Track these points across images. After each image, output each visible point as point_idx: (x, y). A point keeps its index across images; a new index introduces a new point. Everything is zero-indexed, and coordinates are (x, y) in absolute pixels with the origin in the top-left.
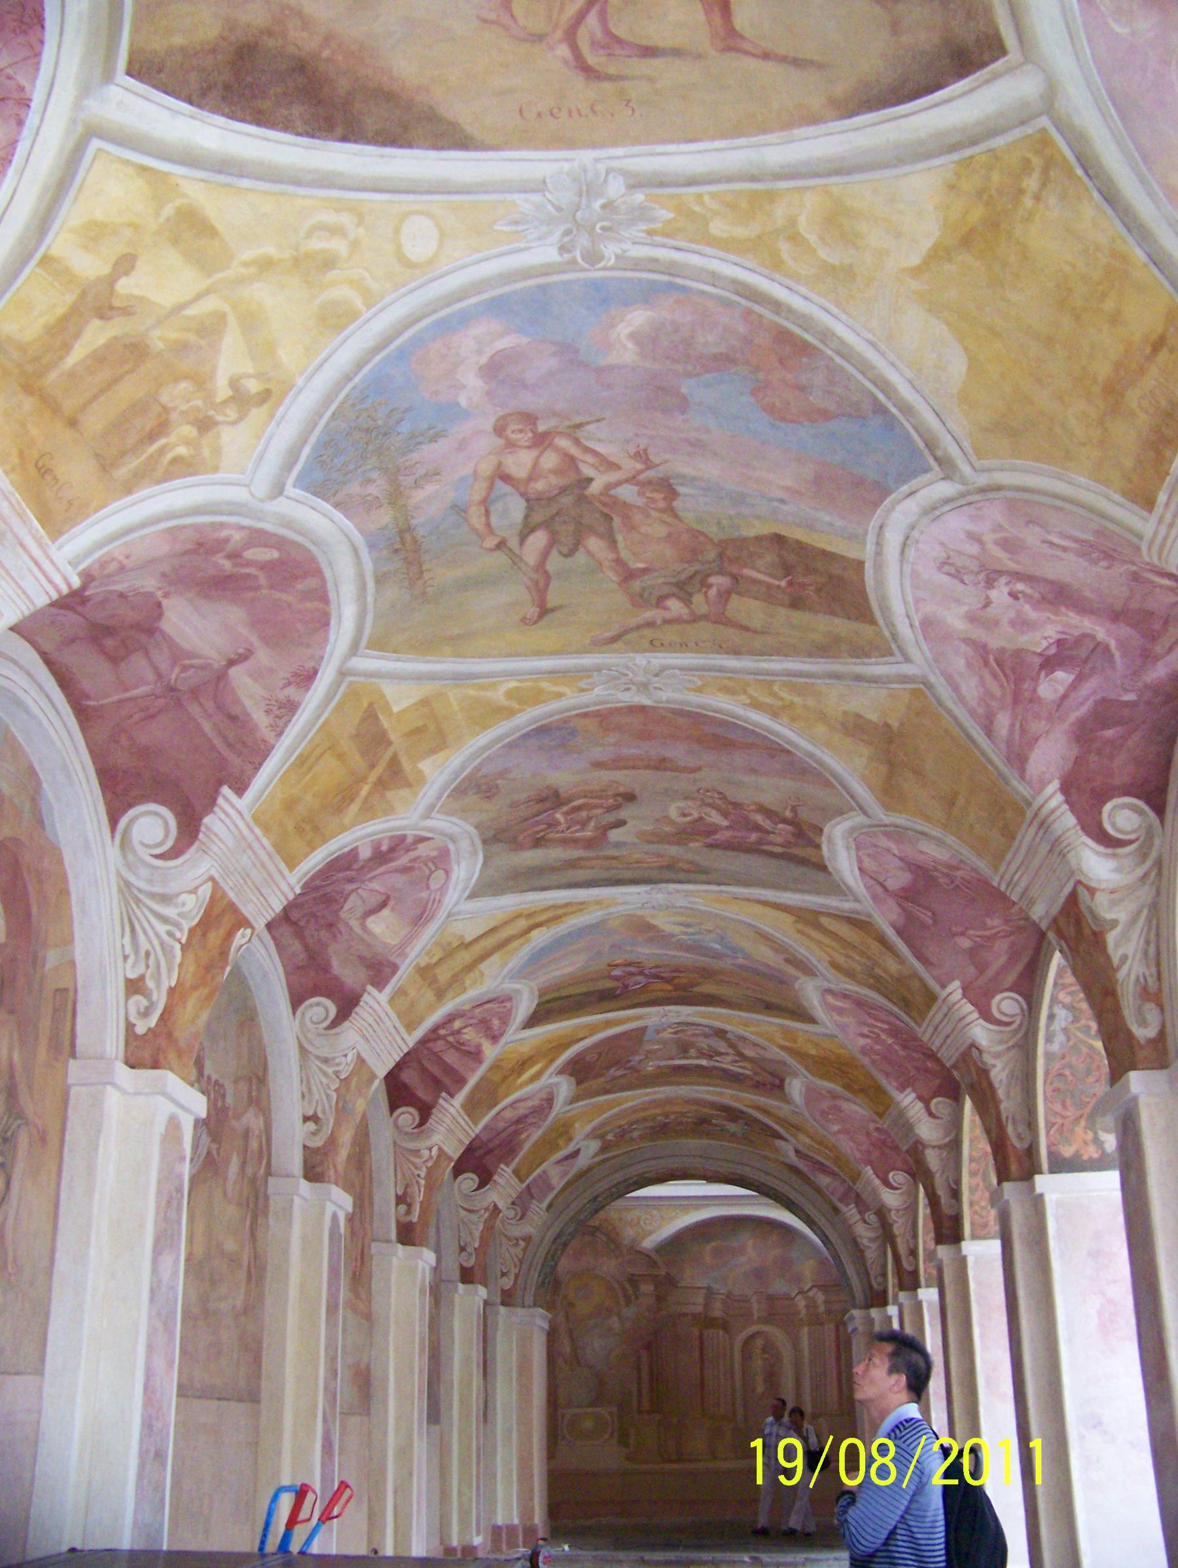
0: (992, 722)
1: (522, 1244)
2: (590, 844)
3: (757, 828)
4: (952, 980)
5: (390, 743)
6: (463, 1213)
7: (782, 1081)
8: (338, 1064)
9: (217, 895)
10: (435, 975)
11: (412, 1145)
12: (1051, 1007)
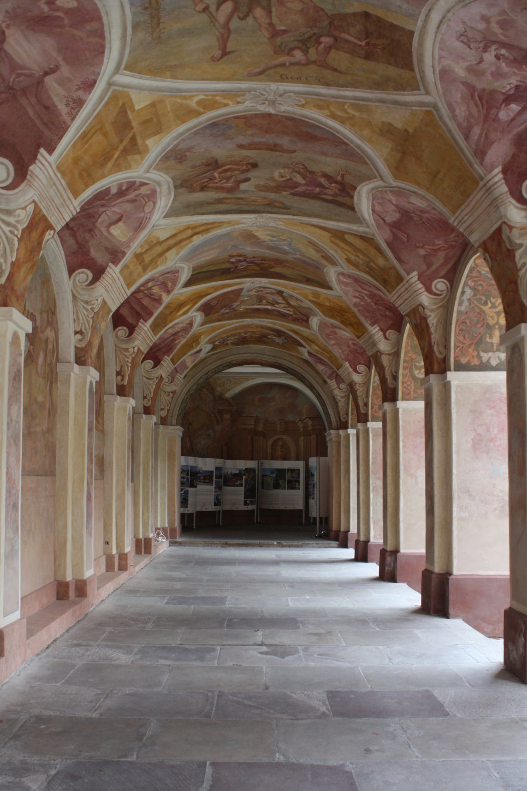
0: (469, 132)
1: (171, 394)
2: (230, 190)
3: (320, 185)
4: (414, 271)
5: (132, 128)
6: (145, 379)
7: (308, 318)
8: (93, 304)
9: (37, 210)
10: (143, 258)
11: (124, 346)
12: (463, 288)
